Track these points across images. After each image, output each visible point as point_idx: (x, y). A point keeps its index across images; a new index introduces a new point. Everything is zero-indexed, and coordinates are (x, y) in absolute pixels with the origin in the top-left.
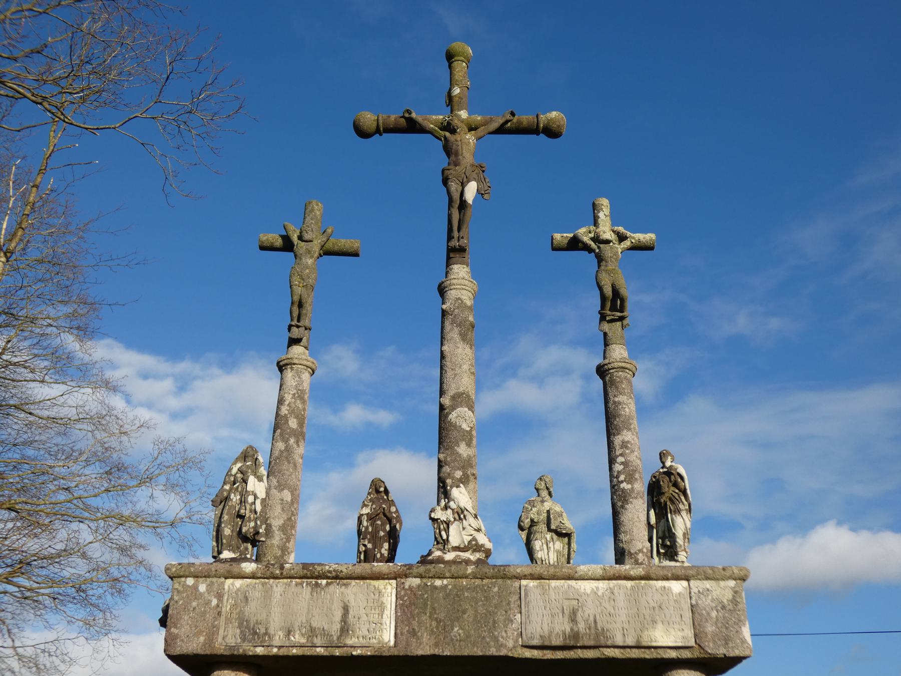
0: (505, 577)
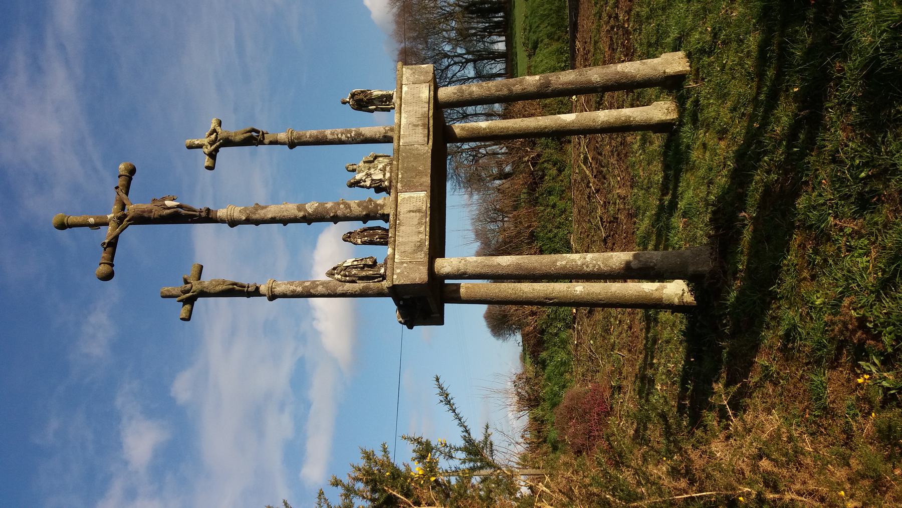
0: (399, 150)
